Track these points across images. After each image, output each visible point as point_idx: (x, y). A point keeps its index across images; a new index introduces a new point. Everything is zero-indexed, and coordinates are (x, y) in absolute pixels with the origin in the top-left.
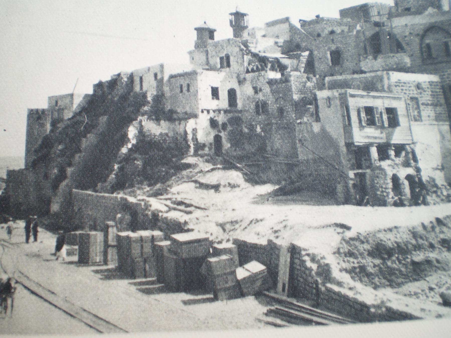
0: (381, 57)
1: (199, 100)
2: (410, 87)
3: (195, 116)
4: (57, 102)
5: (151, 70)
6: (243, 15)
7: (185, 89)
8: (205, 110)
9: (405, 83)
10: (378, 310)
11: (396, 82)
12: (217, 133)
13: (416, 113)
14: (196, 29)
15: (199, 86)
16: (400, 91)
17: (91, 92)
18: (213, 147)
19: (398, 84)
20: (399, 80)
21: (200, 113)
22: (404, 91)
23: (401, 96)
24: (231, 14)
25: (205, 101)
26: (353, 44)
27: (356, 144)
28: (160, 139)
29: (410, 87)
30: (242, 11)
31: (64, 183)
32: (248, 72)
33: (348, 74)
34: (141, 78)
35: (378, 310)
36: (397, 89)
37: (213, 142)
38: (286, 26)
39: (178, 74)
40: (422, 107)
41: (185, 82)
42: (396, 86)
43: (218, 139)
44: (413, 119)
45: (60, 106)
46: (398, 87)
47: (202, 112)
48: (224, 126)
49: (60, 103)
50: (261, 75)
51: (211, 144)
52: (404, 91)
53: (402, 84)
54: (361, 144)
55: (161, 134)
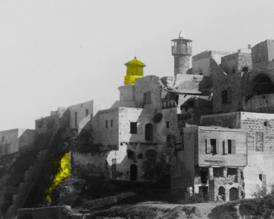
0: (72, 124)
1: (119, 135)
2: (258, 124)
3: (116, 148)
4: (3, 138)
5: (84, 106)
6: (186, 41)
7: (109, 124)
8: (124, 142)
9: (253, 121)
10: (103, 210)
11: (245, 120)
12: (133, 163)
13: (259, 144)
14: (126, 65)
15: (120, 122)
16: (248, 127)
17: (33, 127)
18: (129, 174)
19: (247, 122)
20: (248, 119)
21: (120, 146)
22: (251, 128)
23: (200, 133)
24: (173, 40)
25: (125, 135)
26: (240, 85)
27: (200, 166)
28: (88, 169)
29: (258, 124)
30: (185, 36)
31: (12, 207)
32: (163, 108)
33: (233, 112)
34: (76, 114)
35: (103, 210)
36: (245, 126)
37: (129, 170)
38: (207, 60)
39: (105, 110)
40: (265, 140)
41: (108, 119)
42: (244, 123)
43: (134, 168)
44: (255, 148)
45: (6, 141)
46: (246, 125)
47: (122, 144)
48: (140, 156)
49: (6, 138)
50: (172, 111)
51: (128, 172)
52: (251, 128)
53: (251, 122)
54: (204, 166)
55: (89, 164)
